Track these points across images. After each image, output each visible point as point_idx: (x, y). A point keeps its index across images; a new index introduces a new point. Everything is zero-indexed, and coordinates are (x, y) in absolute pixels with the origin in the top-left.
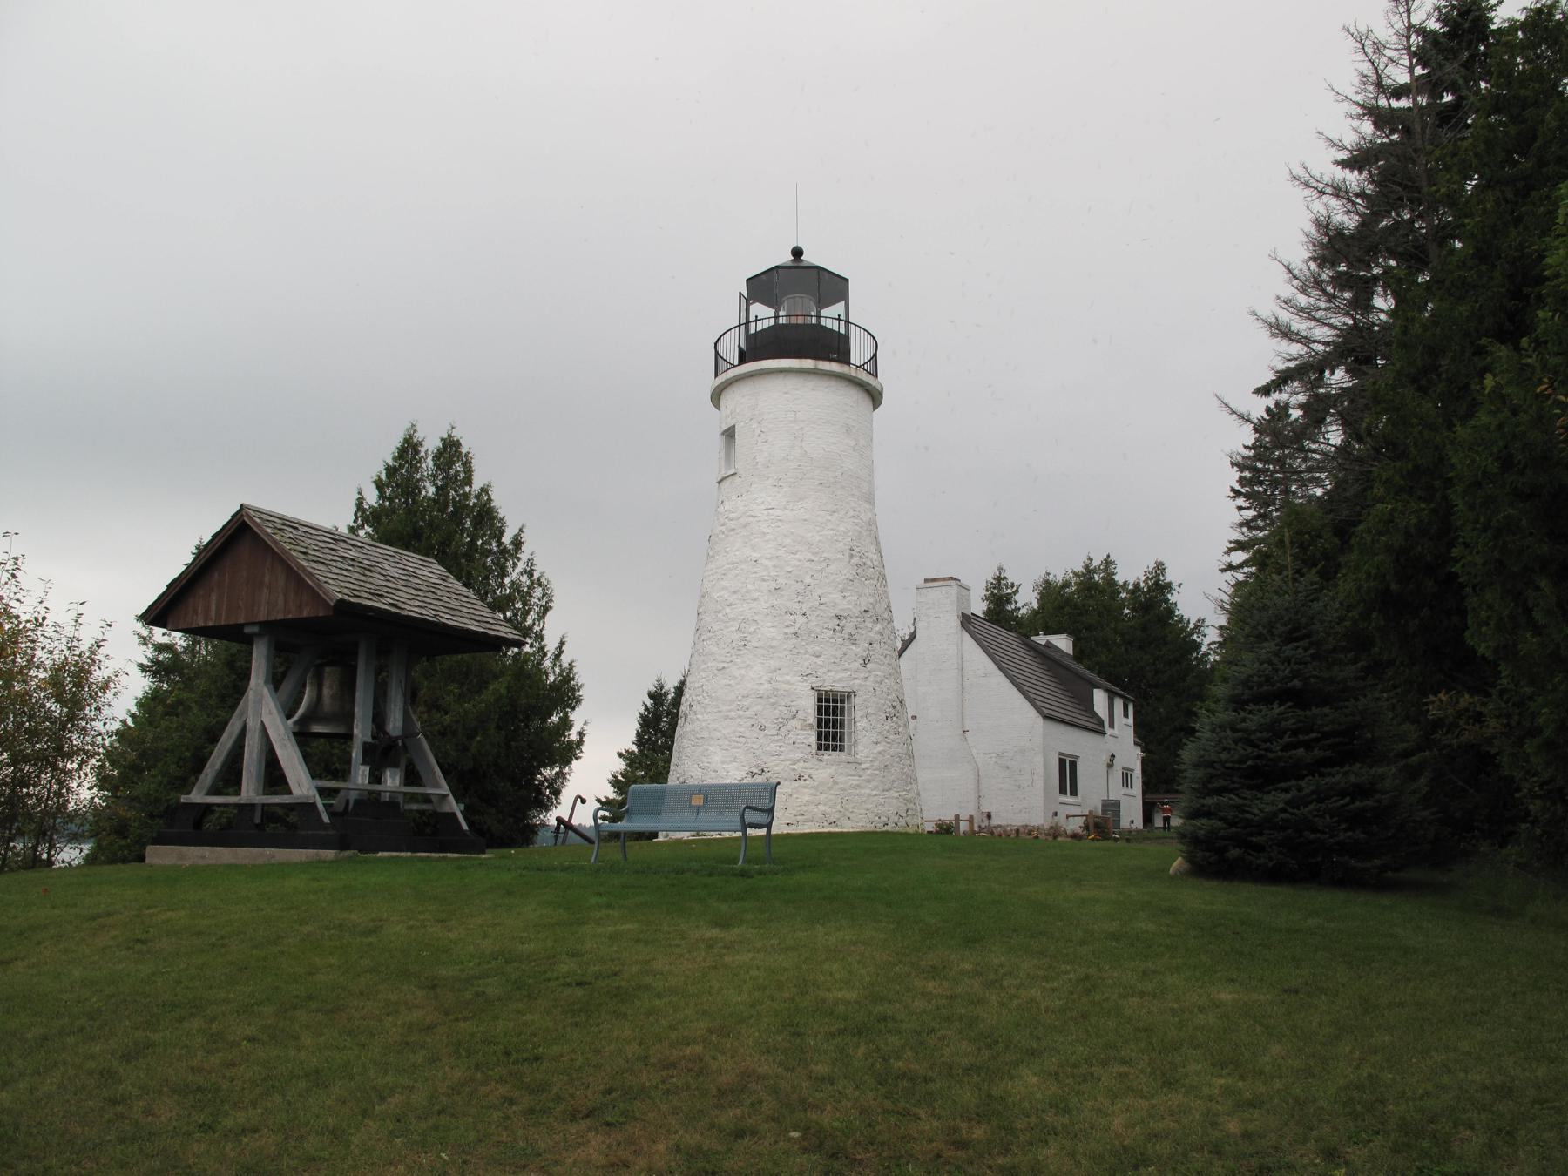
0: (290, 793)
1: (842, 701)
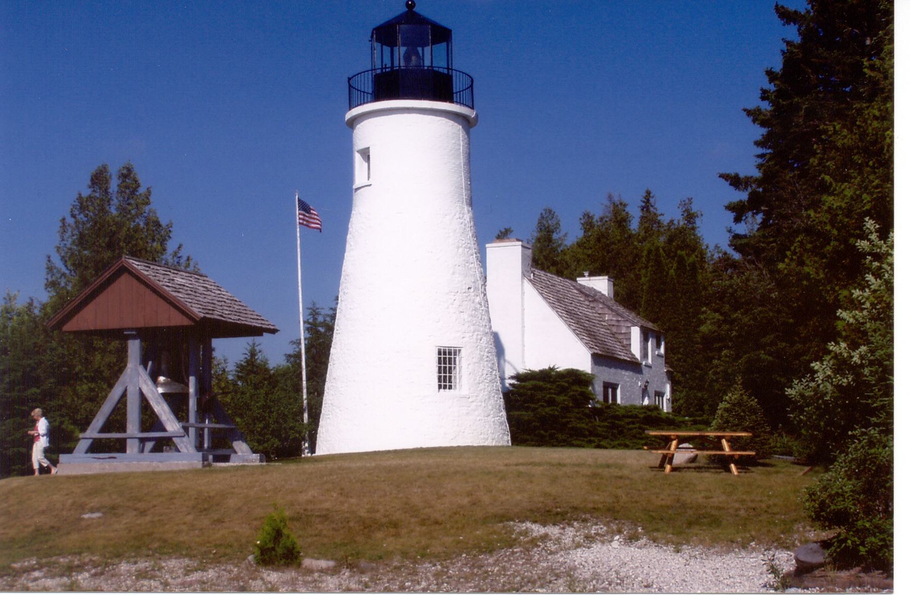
0: (164, 430)
1: (455, 354)
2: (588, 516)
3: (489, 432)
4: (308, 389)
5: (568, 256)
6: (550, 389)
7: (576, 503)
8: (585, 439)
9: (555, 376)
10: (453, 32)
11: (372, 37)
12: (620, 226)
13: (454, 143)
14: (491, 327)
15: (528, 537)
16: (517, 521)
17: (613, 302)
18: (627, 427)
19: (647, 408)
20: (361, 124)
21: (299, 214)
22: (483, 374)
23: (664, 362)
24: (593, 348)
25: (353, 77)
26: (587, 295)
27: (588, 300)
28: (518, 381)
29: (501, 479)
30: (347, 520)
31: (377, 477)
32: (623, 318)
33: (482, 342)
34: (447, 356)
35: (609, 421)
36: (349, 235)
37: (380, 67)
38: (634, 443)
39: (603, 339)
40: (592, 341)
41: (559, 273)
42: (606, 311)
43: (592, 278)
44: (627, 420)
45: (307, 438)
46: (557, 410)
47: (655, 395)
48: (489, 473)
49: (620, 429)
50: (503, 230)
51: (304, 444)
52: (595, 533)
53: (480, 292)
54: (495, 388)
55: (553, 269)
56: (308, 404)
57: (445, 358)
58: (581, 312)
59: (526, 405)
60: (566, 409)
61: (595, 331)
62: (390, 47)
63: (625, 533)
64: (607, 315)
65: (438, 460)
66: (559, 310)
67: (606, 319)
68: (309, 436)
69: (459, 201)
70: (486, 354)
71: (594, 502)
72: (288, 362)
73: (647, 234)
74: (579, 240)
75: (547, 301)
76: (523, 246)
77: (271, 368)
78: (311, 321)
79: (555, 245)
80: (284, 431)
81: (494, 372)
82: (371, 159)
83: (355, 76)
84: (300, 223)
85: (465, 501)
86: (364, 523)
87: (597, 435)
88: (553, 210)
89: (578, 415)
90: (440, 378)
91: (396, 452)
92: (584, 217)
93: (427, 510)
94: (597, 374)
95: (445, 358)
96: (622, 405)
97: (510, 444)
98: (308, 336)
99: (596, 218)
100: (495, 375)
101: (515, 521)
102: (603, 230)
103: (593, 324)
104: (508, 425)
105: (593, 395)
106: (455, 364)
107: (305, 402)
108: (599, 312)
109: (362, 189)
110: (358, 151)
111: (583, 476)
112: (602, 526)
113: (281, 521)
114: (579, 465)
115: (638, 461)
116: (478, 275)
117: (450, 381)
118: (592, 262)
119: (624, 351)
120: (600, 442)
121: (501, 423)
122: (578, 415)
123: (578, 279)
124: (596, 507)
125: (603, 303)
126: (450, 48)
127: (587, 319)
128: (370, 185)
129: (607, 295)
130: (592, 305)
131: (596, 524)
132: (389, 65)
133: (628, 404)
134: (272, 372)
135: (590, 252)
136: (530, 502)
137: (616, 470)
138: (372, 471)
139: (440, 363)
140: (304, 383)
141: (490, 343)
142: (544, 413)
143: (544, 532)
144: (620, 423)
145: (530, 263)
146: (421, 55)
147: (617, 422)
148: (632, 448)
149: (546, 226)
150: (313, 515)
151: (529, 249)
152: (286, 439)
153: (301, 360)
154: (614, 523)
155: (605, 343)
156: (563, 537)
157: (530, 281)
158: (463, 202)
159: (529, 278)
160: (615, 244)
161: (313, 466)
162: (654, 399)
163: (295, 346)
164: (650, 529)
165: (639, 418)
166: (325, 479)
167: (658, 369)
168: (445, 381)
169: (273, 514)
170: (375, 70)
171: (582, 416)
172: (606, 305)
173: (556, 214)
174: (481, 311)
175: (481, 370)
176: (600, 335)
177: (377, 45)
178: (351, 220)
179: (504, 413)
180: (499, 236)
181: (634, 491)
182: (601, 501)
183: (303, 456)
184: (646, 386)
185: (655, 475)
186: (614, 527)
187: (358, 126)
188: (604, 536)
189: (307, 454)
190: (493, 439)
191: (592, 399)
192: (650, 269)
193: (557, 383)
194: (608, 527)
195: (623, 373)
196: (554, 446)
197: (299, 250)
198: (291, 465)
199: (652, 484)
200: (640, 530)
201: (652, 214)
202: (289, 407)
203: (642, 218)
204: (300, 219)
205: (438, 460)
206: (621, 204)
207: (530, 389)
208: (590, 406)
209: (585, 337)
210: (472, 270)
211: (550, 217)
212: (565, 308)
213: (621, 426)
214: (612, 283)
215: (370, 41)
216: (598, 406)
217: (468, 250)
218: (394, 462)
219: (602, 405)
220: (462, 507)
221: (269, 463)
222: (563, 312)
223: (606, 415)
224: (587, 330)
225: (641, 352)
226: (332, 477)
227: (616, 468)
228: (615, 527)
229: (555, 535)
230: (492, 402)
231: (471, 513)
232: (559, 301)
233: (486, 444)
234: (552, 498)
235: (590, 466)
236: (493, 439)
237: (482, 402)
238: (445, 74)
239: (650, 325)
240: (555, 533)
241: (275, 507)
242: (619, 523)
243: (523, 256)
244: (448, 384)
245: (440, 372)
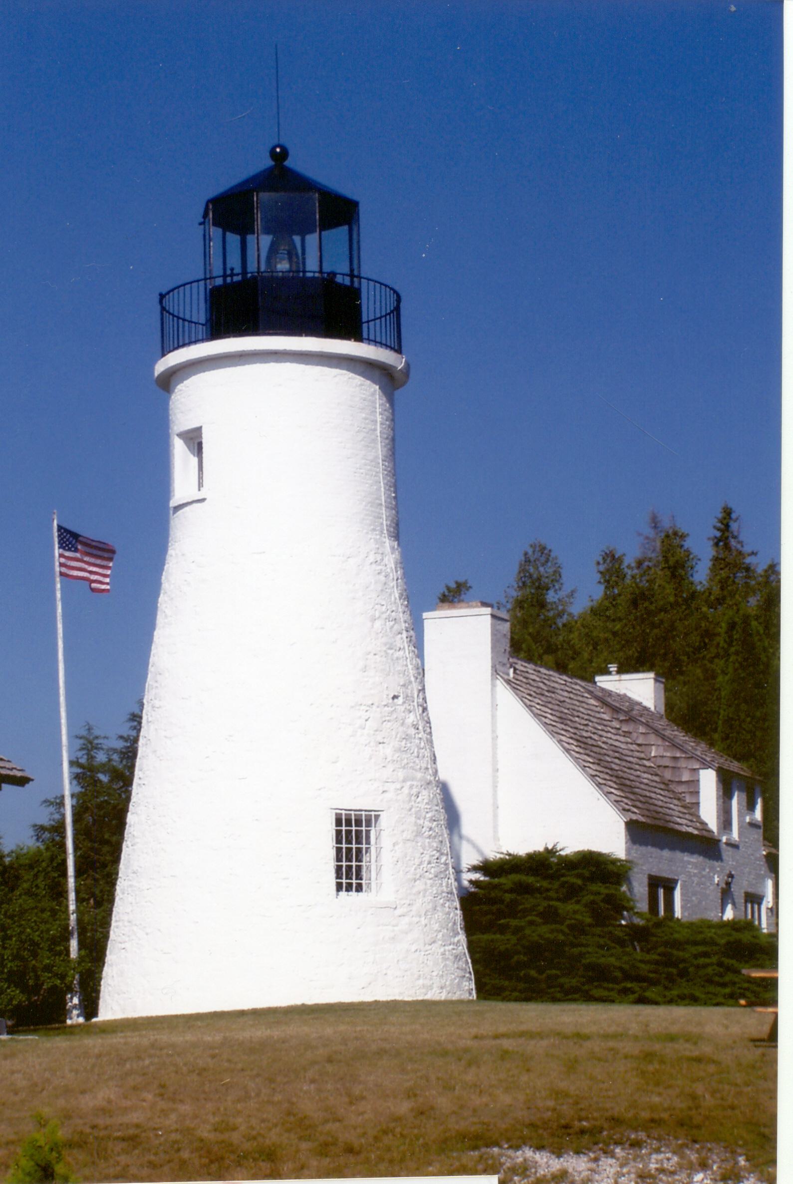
1: (369, 824)
2: (642, 1135)
3: (435, 974)
4: (77, 892)
5: (576, 634)
6: (548, 890)
7: (619, 1109)
8: (616, 986)
9: (558, 864)
10: (360, 205)
11: (205, 215)
12: (673, 576)
13: (366, 419)
14: (436, 771)
15: (529, 1176)
16: (506, 1146)
17: (664, 722)
18: (695, 962)
19: (733, 925)
20: (185, 382)
21: (61, 556)
22: (421, 863)
23: (761, 838)
24: (628, 810)
25: (168, 293)
26: (615, 710)
27: (617, 719)
28: (485, 875)
29: (469, 1064)
30: (176, 1146)
31: (229, 1061)
32: (686, 753)
33: (419, 799)
34: (354, 828)
35: (661, 949)
36: (162, 595)
37: (221, 273)
38: (708, 993)
39: (648, 794)
40: (626, 798)
41: (561, 668)
42: (652, 739)
43: (625, 677)
44: (694, 950)
45: (77, 988)
46: (562, 932)
47: (746, 902)
48: (445, 1053)
49: (681, 966)
50: (453, 585)
51: (72, 998)
52: (657, 1169)
53: (415, 704)
54: (445, 889)
55: (549, 658)
56: (79, 921)
57: (349, 832)
58: (604, 743)
59: (502, 921)
60: (578, 929)
61: (632, 778)
62: (240, 235)
63: (715, 1168)
64: (653, 748)
65: (342, 1028)
66: (563, 738)
67: (653, 754)
68: (82, 983)
69: (374, 530)
70: (427, 824)
71: (653, 1108)
72: (37, 840)
73: (725, 593)
74: (595, 603)
75: (539, 720)
76: (493, 616)
77: (6, 852)
78: (83, 761)
79: (551, 614)
80: (32, 974)
81: (443, 859)
82: (204, 450)
83: (173, 290)
84: (62, 574)
85: (404, 1107)
86: (209, 1152)
87: (639, 979)
88: (549, 547)
89: (602, 941)
90: (339, 869)
91: (256, 1013)
92: (604, 560)
93: (329, 1127)
94: (635, 860)
95: (349, 832)
96: (684, 920)
97: (475, 997)
98: (78, 789)
99: (629, 560)
100: (446, 864)
101: (501, 1147)
102: (644, 584)
103: (629, 765)
104: (469, 961)
105: (629, 900)
106: (368, 842)
107: (73, 917)
108: (639, 742)
109: (187, 509)
110: (180, 435)
111: (626, 1057)
112: (669, 1155)
113: (52, 1150)
114: (615, 1036)
115: (727, 1027)
116: (412, 672)
117: (359, 876)
118: (623, 646)
119: (687, 816)
120: (644, 991)
121: (457, 958)
122: (602, 941)
123: (598, 679)
124: (656, 1116)
125: (647, 725)
126: (355, 236)
127: (617, 755)
128: (203, 500)
129: (653, 709)
130: (625, 728)
131: (658, 1151)
132: (238, 270)
133: (695, 918)
134: (7, 860)
135: (618, 626)
136: (529, 1108)
137: (687, 1046)
138: (217, 1051)
139: (339, 841)
140: (71, 881)
141: (435, 802)
142: (536, 938)
143: (558, 1167)
144: (681, 954)
145: (508, 649)
146: (300, 252)
147: (675, 952)
148: (705, 1004)
149: (535, 576)
150: (109, 1137)
151: (506, 621)
152: (38, 987)
153: (64, 837)
154: (692, 1149)
155: (651, 801)
156: (597, 1177)
157: (508, 682)
158: (382, 532)
159: (506, 677)
160: (666, 611)
161: (100, 1040)
162: (743, 908)
163: (52, 809)
164: (761, 1160)
165: (716, 944)
166: (128, 1066)
167: (750, 851)
168: (349, 877)
169: (37, 1136)
170: (210, 278)
171: (609, 942)
172: (652, 728)
173: (553, 554)
174: (417, 741)
175: (418, 855)
176: (643, 786)
177: (215, 232)
178: (166, 567)
179: (462, 937)
180: (444, 595)
181: (727, 1087)
182: (666, 1105)
183: (69, 1022)
184: (728, 884)
185: (764, 1055)
186: (692, 1157)
187: (179, 387)
188: (673, 1173)
189: (76, 1019)
190: (442, 988)
191: (629, 909)
192: (733, 658)
193: (563, 879)
194: (682, 1156)
195: (686, 858)
196: (554, 1000)
197: (60, 626)
198: (58, 1039)
199: (760, 1073)
200: (742, 1161)
201: (735, 553)
202: (43, 927)
203: (716, 559)
204: (61, 565)
205: (342, 1028)
206: (675, 534)
207: (511, 891)
208: (623, 922)
209: (613, 790)
210: (401, 661)
211: (543, 559)
212: (575, 734)
213: (684, 961)
214: (662, 686)
215: (200, 224)
216: (637, 921)
217: (392, 623)
218: (260, 1033)
219: (648, 920)
220: (398, 1119)
221: (16, 1037)
222: (571, 741)
223: (654, 939)
224: (617, 777)
225: (718, 818)
226: (141, 1063)
227: (687, 1041)
228: (694, 1157)
229: (580, 1172)
230: (440, 915)
231: (416, 1131)
232: (562, 720)
233: (429, 997)
234: (571, 1101)
235: (636, 1038)
236: (442, 988)
237: (420, 916)
238: (345, 286)
239: (734, 766)
240: (581, 1169)
241: (42, 1123)
242: (702, 1148)
243: (494, 634)
244: (354, 881)
245: (339, 859)
